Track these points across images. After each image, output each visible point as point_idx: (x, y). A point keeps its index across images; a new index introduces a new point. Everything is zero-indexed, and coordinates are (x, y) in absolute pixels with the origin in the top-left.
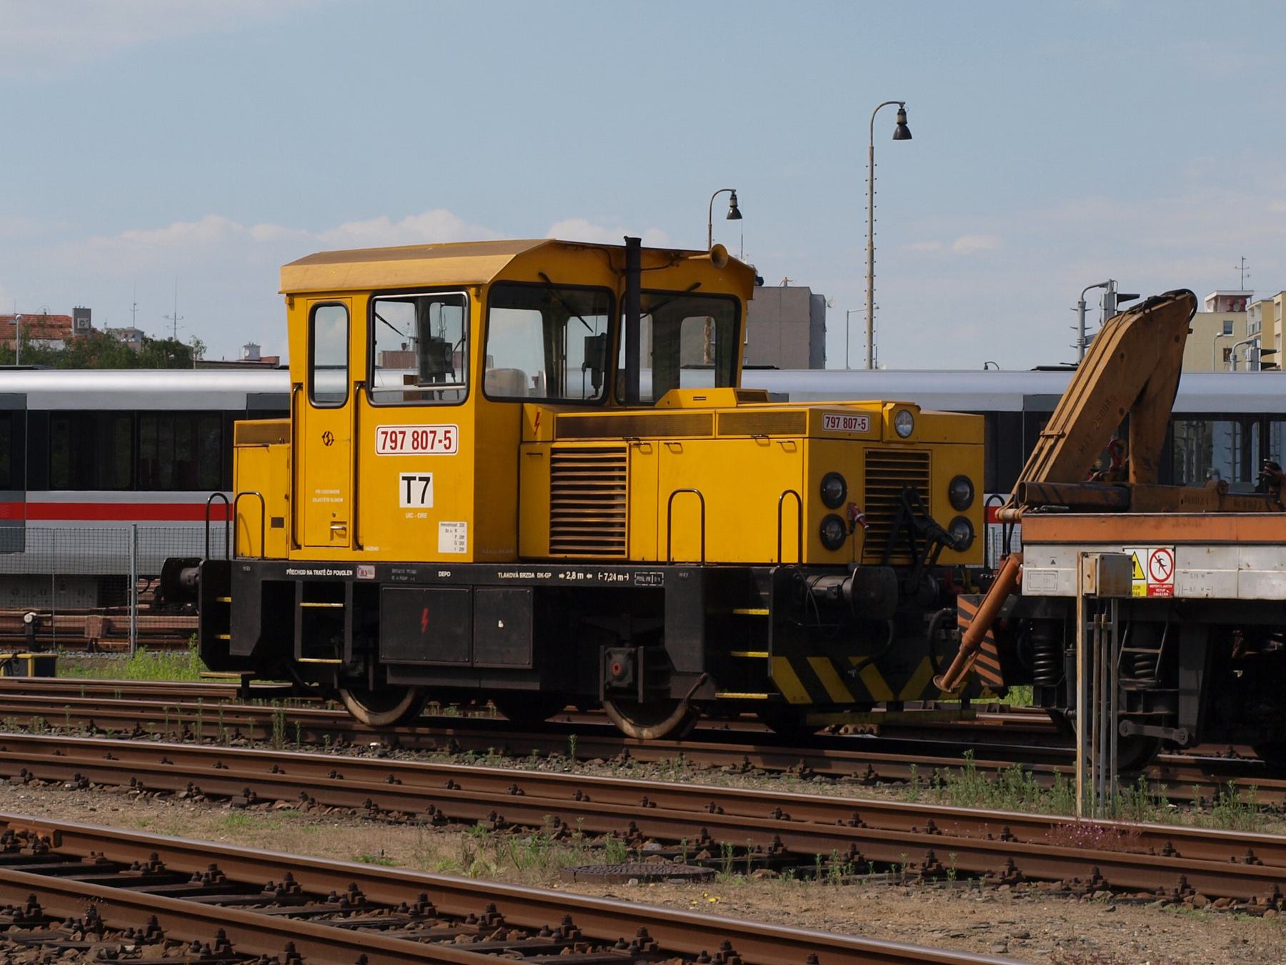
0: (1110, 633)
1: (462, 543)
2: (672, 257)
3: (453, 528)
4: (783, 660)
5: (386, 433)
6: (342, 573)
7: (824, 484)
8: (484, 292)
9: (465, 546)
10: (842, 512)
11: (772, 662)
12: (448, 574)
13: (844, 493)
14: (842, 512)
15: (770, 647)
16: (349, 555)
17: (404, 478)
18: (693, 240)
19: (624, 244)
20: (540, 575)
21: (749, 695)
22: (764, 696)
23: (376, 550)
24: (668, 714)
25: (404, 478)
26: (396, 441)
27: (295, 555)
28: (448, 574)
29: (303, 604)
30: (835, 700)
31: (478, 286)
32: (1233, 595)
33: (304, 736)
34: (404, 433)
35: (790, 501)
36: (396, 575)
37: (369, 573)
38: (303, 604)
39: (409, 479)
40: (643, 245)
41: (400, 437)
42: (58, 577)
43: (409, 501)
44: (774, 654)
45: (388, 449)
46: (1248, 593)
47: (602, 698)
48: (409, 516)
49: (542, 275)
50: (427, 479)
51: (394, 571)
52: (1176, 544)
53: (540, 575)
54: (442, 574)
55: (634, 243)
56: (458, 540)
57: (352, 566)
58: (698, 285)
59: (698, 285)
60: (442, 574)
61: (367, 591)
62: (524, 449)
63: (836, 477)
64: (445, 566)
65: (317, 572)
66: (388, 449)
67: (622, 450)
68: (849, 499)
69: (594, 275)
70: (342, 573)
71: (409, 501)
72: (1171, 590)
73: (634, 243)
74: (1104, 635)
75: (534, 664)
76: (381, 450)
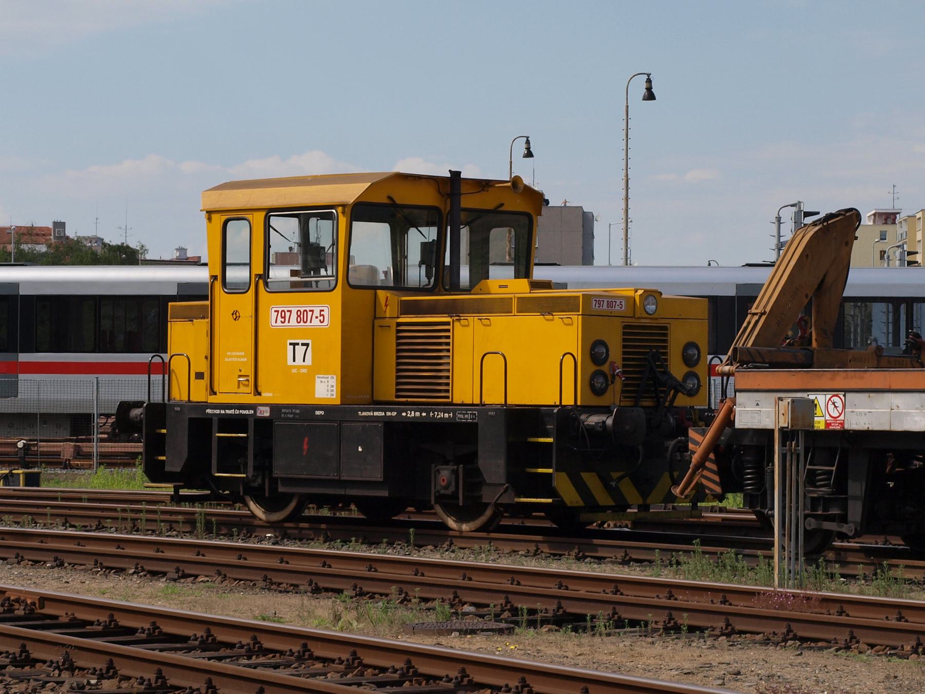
0: (798, 455)
1: (332, 391)
2: (484, 185)
3: (326, 380)
4: (563, 475)
5: (278, 311)
6: (246, 412)
7: (593, 348)
8: (348, 210)
9: (334, 393)
10: (605, 368)
11: (555, 476)
12: (322, 413)
13: (607, 355)
14: (605, 368)
15: (554, 465)
16: (251, 399)
17: (291, 344)
18: (499, 173)
19: (449, 175)
20: (389, 414)
21: (538, 500)
22: (550, 500)
23: (270, 395)
24: (480, 513)
25: (291, 344)
26: (284, 317)
27: (212, 399)
28: (322, 413)
29: (218, 435)
30: (601, 504)
31: (344, 206)
32: (887, 428)
33: (218, 529)
34: (290, 311)
35: (569, 361)
36: (285, 413)
37: (265, 412)
38: (218, 435)
39: (294, 345)
40: (462, 176)
41: (288, 314)
42: (42, 415)
43: (294, 361)
44: (557, 470)
45: (279, 323)
46: (898, 427)
47: (433, 502)
48: (294, 371)
49: (390, 198)
50: (307, 345)
51: (283, 411)
52: (846, 391)
53: (389, 414)
54: (318, 413)
55: (456, 175)
56: (330, 388)
57: (253, 407)
58: (502, 205)
59: (502, 205)
60: (318, 413)
61: (264, 425)
62: (377, 323)
63: (601, 343)
64: (320, 407)
65: (228, 412)
66: (279, 323)
67: (448, 324)
68: (610, 359)
69: (427, 198)
70: (246, 412)
71: (294, 361)
72: (842, 424)
73: (456, 175)
74: (794, 457)
75: (384, 478)
76: (274, 324)
